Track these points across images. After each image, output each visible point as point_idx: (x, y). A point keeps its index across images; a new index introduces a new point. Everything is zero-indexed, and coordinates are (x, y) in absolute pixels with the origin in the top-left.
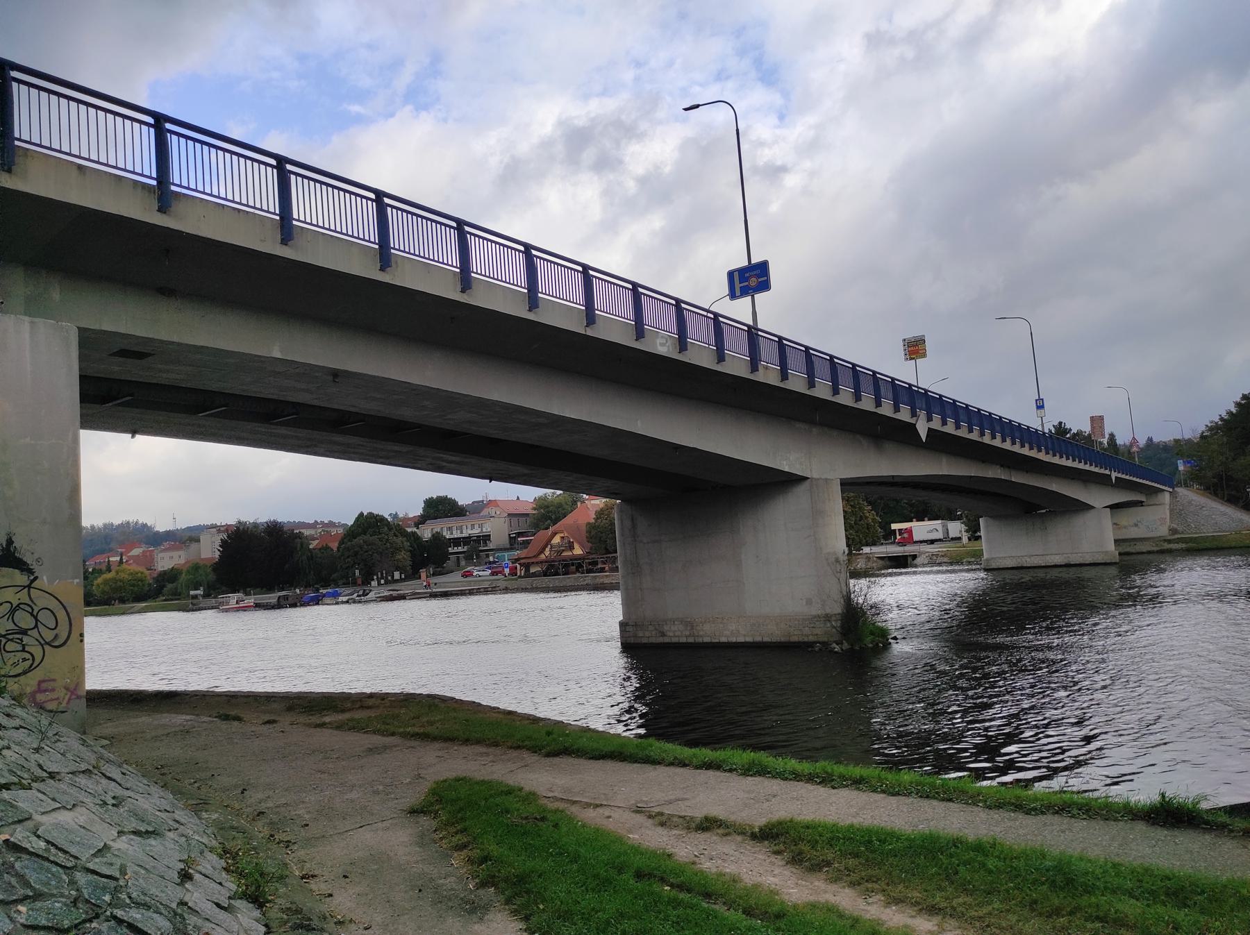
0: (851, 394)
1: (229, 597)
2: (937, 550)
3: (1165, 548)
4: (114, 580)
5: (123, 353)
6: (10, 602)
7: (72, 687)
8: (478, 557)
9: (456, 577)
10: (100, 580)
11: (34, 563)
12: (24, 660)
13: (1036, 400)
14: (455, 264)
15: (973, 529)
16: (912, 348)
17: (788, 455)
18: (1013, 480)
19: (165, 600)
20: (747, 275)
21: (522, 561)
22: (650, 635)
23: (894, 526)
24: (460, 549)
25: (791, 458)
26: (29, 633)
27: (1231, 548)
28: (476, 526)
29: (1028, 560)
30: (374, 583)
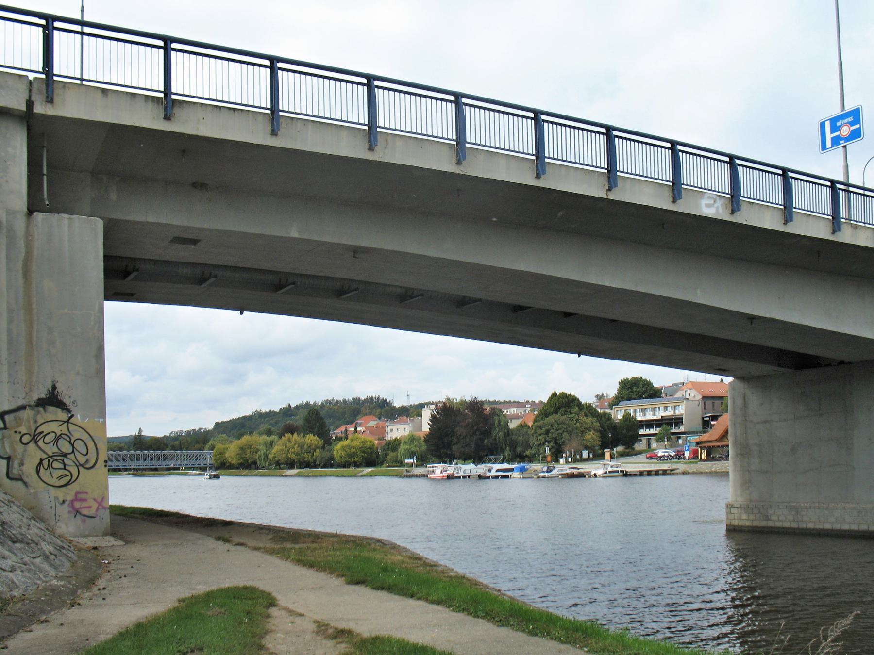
1: (435, 467)
4: (349, 446)
5: (179, 240)
6: (56, 433)
7: (99, 499)
10: (339, 446)
11: (71, 404)
12: (66, 475)
19: (389, 466)
20: (839, 124)
21: (703, 445)
24: (652, 431)
26: (69, 456)
28: (669, 409)
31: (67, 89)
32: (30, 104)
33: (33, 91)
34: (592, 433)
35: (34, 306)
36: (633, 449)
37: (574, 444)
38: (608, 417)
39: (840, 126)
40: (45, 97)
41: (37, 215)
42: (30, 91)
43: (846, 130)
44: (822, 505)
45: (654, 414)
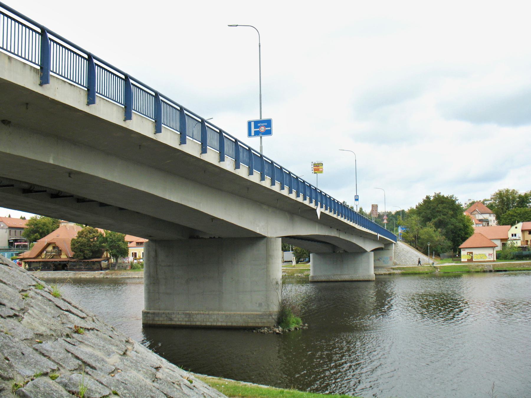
0: (122, 110)
3: (391, 272)
13: (355, 196)
14: (85, 85)
15: (299, 258)
16: (316, 168)
18: (341, 237)
20: (259, 125)
27: (419, 274)
29: (332, 277)
39: (260, 126)
43: (263, 129)
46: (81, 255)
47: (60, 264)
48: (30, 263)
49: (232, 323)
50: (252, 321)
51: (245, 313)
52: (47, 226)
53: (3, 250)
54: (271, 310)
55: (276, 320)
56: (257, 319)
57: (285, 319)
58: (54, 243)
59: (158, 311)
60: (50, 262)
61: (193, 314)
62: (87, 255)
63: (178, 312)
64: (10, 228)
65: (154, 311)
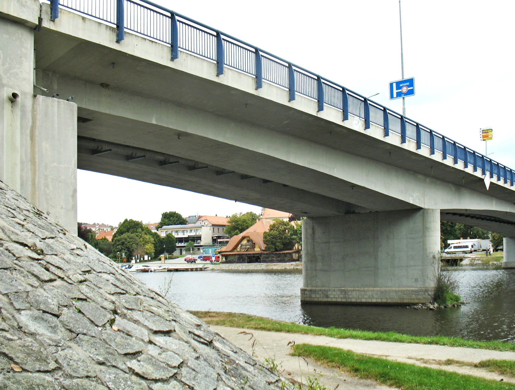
0: (213, 66)
2: (475, 256)
5: (18, 200)
8: (193, 250)
9: (181, 260)
14: (287, 87)
15: (496, 245)
16: (484, 134)
17: (413, 194)
20: (401, 85)
22: (319, 296)
23: (449, 242)
24: (182, 244)
25: (414, 196)
28: (193, 231)
30: (133, 261)
31: (62, 14)
32: (40, 20)
33: (42, 12)
34: (149, 245)
35: (37, 160)
36: (173, 255)
37: (140, 251)
38: (156, 235)
39: (402, 87)
40: (50, 17)
41: (39, 97)
42: (41, 11)
44: (360, 289)
45: (184, 234)
46: (272, 247)
47: (254, 257)
48: (226, 256)
49: (387, 299)
50: (407, 297)
51: (400, 289)
52: (247, 223)
53: (207, 246)
54: (427, 285)
55: (433, 296)
56: (412, 295)
57: (441, 295)
58: (248, 237)
59: (315, 288)
60: (244, 254)
61: (349, 291)
62: (278, 247)
63: (334, 289)
64: (213, 225)
65: (311, 288)
